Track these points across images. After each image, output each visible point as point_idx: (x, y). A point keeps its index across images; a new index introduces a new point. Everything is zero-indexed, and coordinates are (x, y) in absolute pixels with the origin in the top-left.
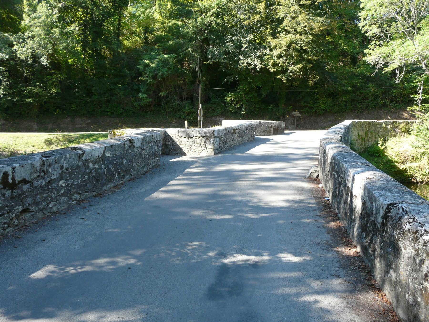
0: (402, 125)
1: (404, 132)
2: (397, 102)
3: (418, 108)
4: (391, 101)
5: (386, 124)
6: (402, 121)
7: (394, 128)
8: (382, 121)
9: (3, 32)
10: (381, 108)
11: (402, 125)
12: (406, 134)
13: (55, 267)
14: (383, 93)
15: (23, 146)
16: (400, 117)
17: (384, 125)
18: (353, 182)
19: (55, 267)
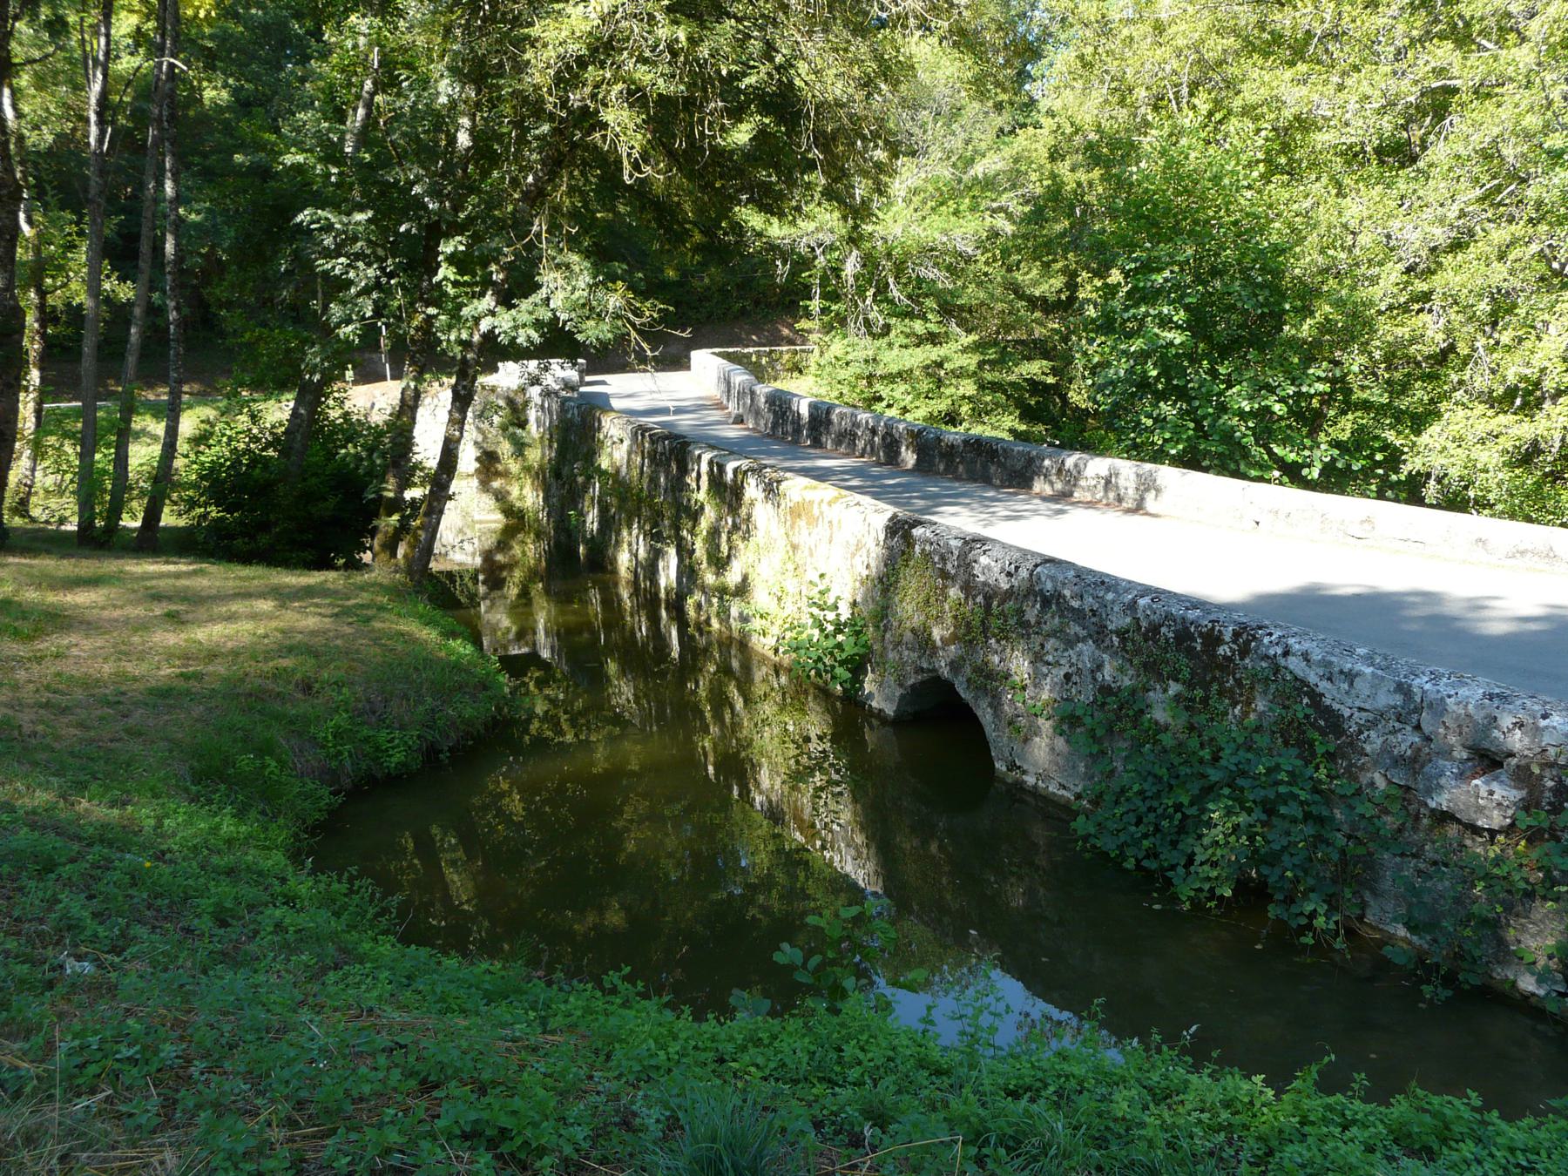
0: (786, 357)
1: (791, 370)
2: (768, 305)
3: (813, 325)
4: (757, 303)
5: (758, 354)
6: (785, 348)
7: (772, 362)
8: (751, 350)
9: (623, 618)
10: (736, 318)
11: (786, 357)
12: (795, 374)
13: (1480, 625)
14: (739, 287)
15: (739, 1103)
16: (777, 340)
17: (754, 359)
18: (1008, 518)
19: (1480, 625)
